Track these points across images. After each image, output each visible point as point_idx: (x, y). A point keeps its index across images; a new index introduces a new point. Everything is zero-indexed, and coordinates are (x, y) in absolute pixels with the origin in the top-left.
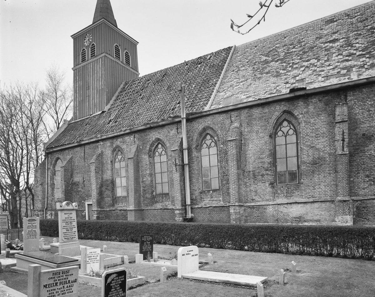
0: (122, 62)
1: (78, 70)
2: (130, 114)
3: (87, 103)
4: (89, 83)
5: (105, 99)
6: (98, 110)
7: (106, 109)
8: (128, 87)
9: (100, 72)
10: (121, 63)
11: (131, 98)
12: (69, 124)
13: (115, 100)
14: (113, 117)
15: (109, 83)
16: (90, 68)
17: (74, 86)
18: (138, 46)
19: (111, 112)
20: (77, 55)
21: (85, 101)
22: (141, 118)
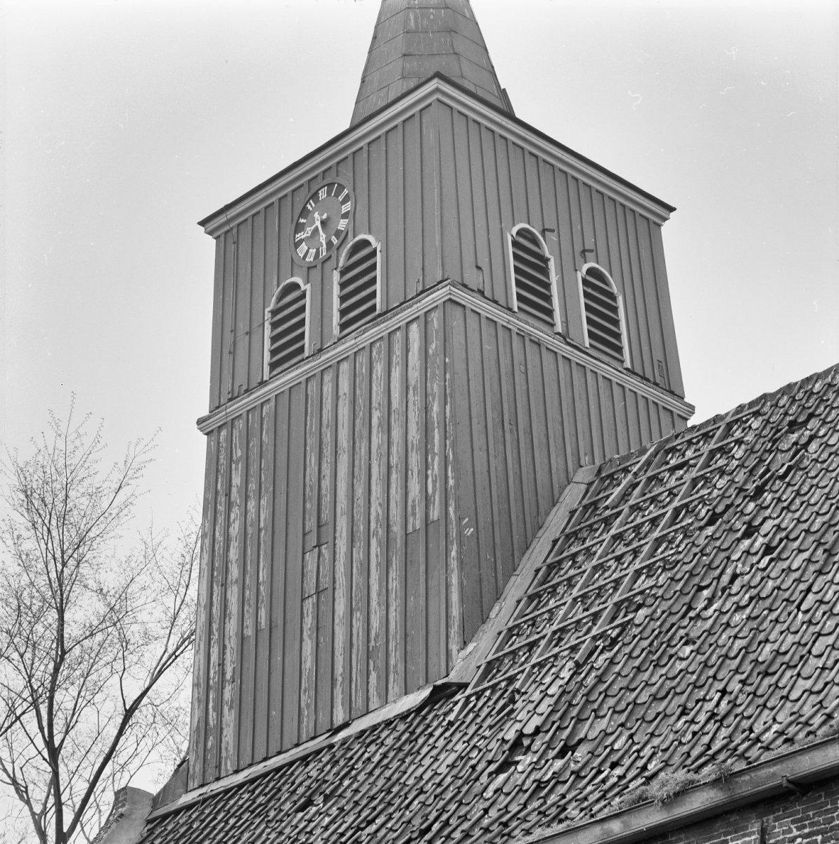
0: (564, 337)
1: (240, 424)
2: (685, 671)
3: (308, 647)
4: (327, 500)
5: (455, 597)
6: (394, 688)
7: (465, 664)
8: (625, 496)
9: (414, 417)
10: (558, 344)
11: (668, 565)
12: (155, 822)
13: (531, 598)
14: (534, 712)
15: (481, 478)
16: (337, 397)
17: (209, 535)
18: (670, 231)
19: (511, 680)
20: (242, 326)
21: (293, 627)
22: (803, 684)
